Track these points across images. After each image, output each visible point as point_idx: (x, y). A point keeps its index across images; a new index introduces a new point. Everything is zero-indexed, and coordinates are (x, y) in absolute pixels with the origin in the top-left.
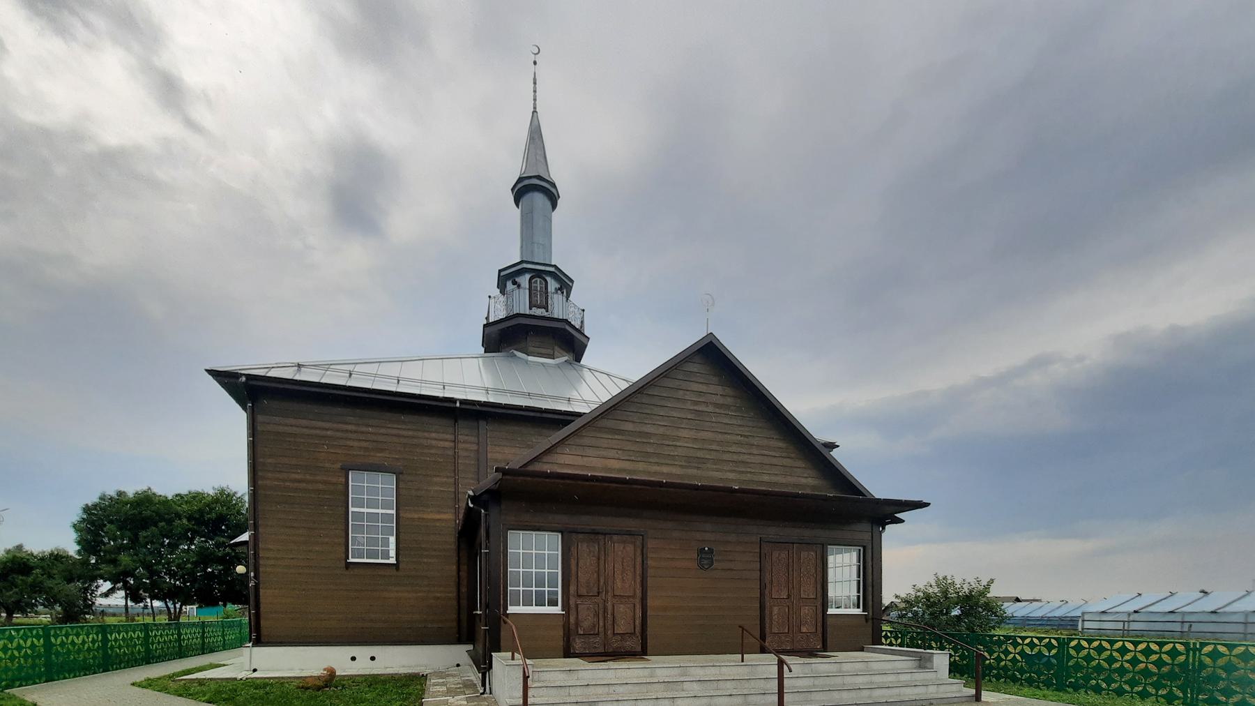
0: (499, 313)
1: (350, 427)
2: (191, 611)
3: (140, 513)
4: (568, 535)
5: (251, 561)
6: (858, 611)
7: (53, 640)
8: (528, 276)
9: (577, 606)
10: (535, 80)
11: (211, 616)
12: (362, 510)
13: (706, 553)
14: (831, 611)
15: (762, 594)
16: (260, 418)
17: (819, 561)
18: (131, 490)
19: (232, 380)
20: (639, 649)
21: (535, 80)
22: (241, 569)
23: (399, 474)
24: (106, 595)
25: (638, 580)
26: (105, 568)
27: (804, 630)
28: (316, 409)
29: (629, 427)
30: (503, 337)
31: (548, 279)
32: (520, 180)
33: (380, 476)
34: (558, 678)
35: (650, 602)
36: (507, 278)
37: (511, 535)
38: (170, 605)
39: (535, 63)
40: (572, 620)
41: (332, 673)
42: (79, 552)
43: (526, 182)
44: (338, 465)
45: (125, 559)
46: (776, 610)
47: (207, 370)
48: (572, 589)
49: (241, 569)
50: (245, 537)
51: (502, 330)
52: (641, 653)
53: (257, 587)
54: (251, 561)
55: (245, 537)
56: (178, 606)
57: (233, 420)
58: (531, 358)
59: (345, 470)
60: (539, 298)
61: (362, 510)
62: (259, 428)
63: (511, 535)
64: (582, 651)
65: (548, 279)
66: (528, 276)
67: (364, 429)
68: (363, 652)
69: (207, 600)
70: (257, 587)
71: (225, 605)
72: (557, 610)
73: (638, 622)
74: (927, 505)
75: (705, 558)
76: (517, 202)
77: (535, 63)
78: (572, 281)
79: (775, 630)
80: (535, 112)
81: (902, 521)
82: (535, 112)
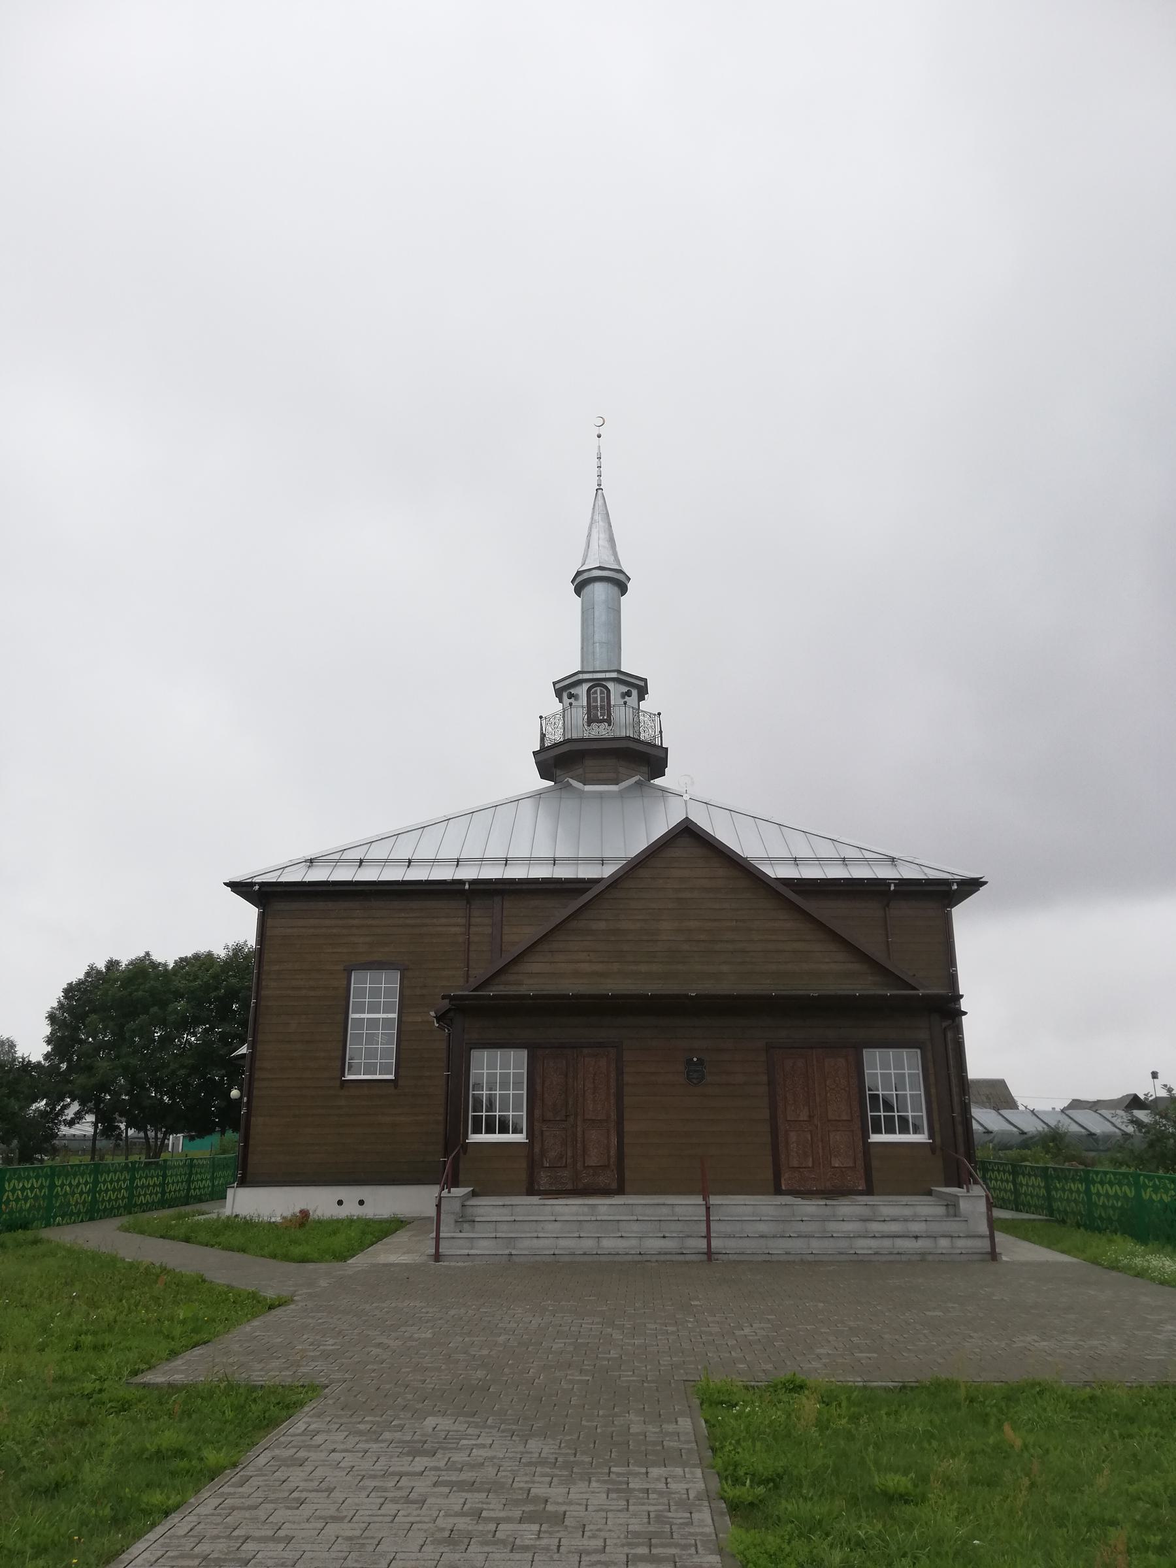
0: (556, 735)
1: (356, 922)
2: (176, 1142)
3: (130, 994)
4: (534, 1050)
5: (245, 1087)
8: (585, 687)
9: (542, 1132)
11: (205, 1148)
13: (695, 1064)
15: (773, 1118)
16: (270, 922)
17: (539, 1088)
18: (125, 957)
19: (249, 889)
20: (614, 1186)
23: (404, 971)
24: (71, 1123)
26: (79, 1079)
27: (836, 1163)
28: (321, 905)
29: (602, 925)
31: (610, 685)
32: (579, 573)
33: (383, 975)
34: (496, 1214)
35: (628, 1127)
36: (564, 689)
37: (475, 1054)
38: (151, 1134)
40: (537, 1150)
41: (305, 1214)
42: (47, 1056)
43: (585, 576)
44: (340, 967)
45: (103, 1063)
46: (793, 1136)
48: (537, 1113)
49: (235, 1093)
50: (243, 1050)
53: (248, 1114)
54: (245, 1087)
55: (243, 1050)
56: (160, 1135)
57: (250, 913)
58: (588, 788)
59: (348, 971)
60: (598, 713)
61: (362, 1016)
62: (268, 933)
63: (475, 1054)
64: (548, 1187)
65: (610, 685)
66: (585, 687)
67: (370, 922)
68: (350, 1193)
69: (198, 1127)
70: (248, 1114)
71: (223, 1133)
72: (520, 1138)
73: (613, 1152)
75: (695, 1072)
78: (645, 680)
79: (795, 1163)
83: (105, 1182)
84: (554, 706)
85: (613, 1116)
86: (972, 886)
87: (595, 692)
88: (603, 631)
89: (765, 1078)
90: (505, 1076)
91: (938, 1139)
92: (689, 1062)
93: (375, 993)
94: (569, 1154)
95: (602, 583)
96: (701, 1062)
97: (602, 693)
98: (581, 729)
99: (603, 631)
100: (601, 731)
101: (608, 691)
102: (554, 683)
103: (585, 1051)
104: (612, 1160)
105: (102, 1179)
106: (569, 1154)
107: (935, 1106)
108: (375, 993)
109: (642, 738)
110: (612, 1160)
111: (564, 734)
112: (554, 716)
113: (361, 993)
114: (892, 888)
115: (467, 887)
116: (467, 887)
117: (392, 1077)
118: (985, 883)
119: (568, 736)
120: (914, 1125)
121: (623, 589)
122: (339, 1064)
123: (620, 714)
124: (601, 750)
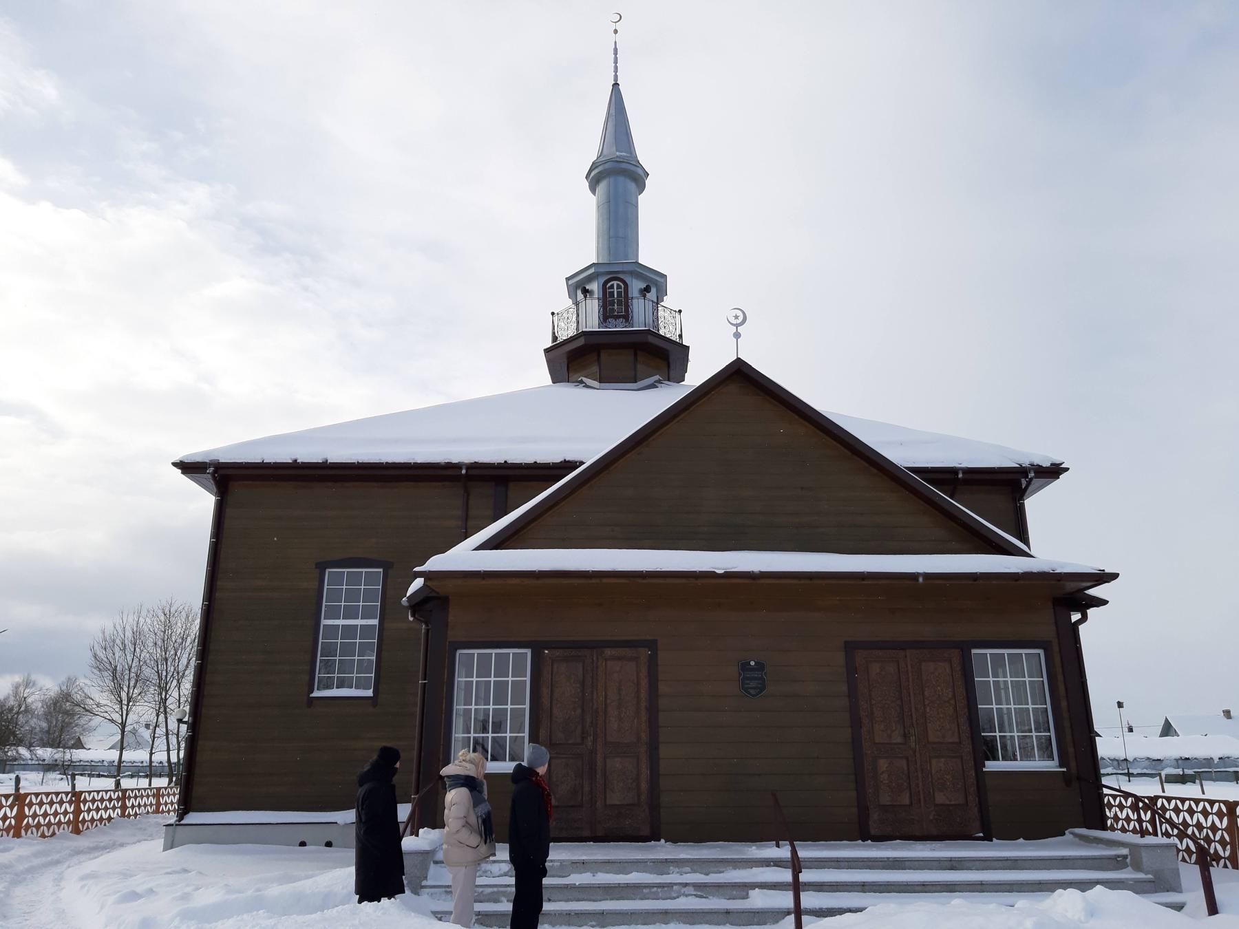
6: (1051, 765)
7: (26, 809)
10: (616, 50)
12: (336, 622)
13: (752, 669)
14: (991, 766)
16: (229, 512)
17: (546, 701)
20: (646, 831)
21: (616, 50)
22: (752, 663)
25: (644, 716)
30: (575, 359)
35: (664, 751)
39: (616, 32)
46: (883, 764)
47: (175, 464)
49: (752, 663)
51: (570, 352)
52: (653, 836)
59: (322, 567)
61: (336, 622)
65: (628, 280)
73: (644, 786)
74: (1114, 576)
76: (593, 189)
77: (616, 32)
79: (885, 799)
80: (616, 85)
81: (1102, 602)
82: (616, 85)
83: (166, 804)
84: (564, 302)
85: (644, 737)
86: (1054, 471)
87: (612, 286)
88: (619, 222)
89: (844, 688)
90: (500, 714)
91: (1073, 764)
92: (745, 666)
93: (352, 595)
94: (586, 789)
95: (618, 175)
96: (760, 666)
97: (619, 287)
98: (592, 322)
99: (619, 222)
100: (457, 892)
101: (626, 285)
102: (568, 279)
103: (608, 652)
104: (643, 798)
105: (129, 804)
106: (586, 789)
107: (1067, 724)
108: (352, 595)
109: (661, 332)
110: (643, 798)
111: (577, 329)
112: (567, 311)
113: (335, 596)
114: (960, 476)
115: (464, 472)
116: (464, 472)
117: (370, 693)
118: (1067, 469)
119: (583, 329)
120: (1004, 747)
121: (641, 187)
122: (307, 678)
123: (639, 308)
124: (614, 339)
